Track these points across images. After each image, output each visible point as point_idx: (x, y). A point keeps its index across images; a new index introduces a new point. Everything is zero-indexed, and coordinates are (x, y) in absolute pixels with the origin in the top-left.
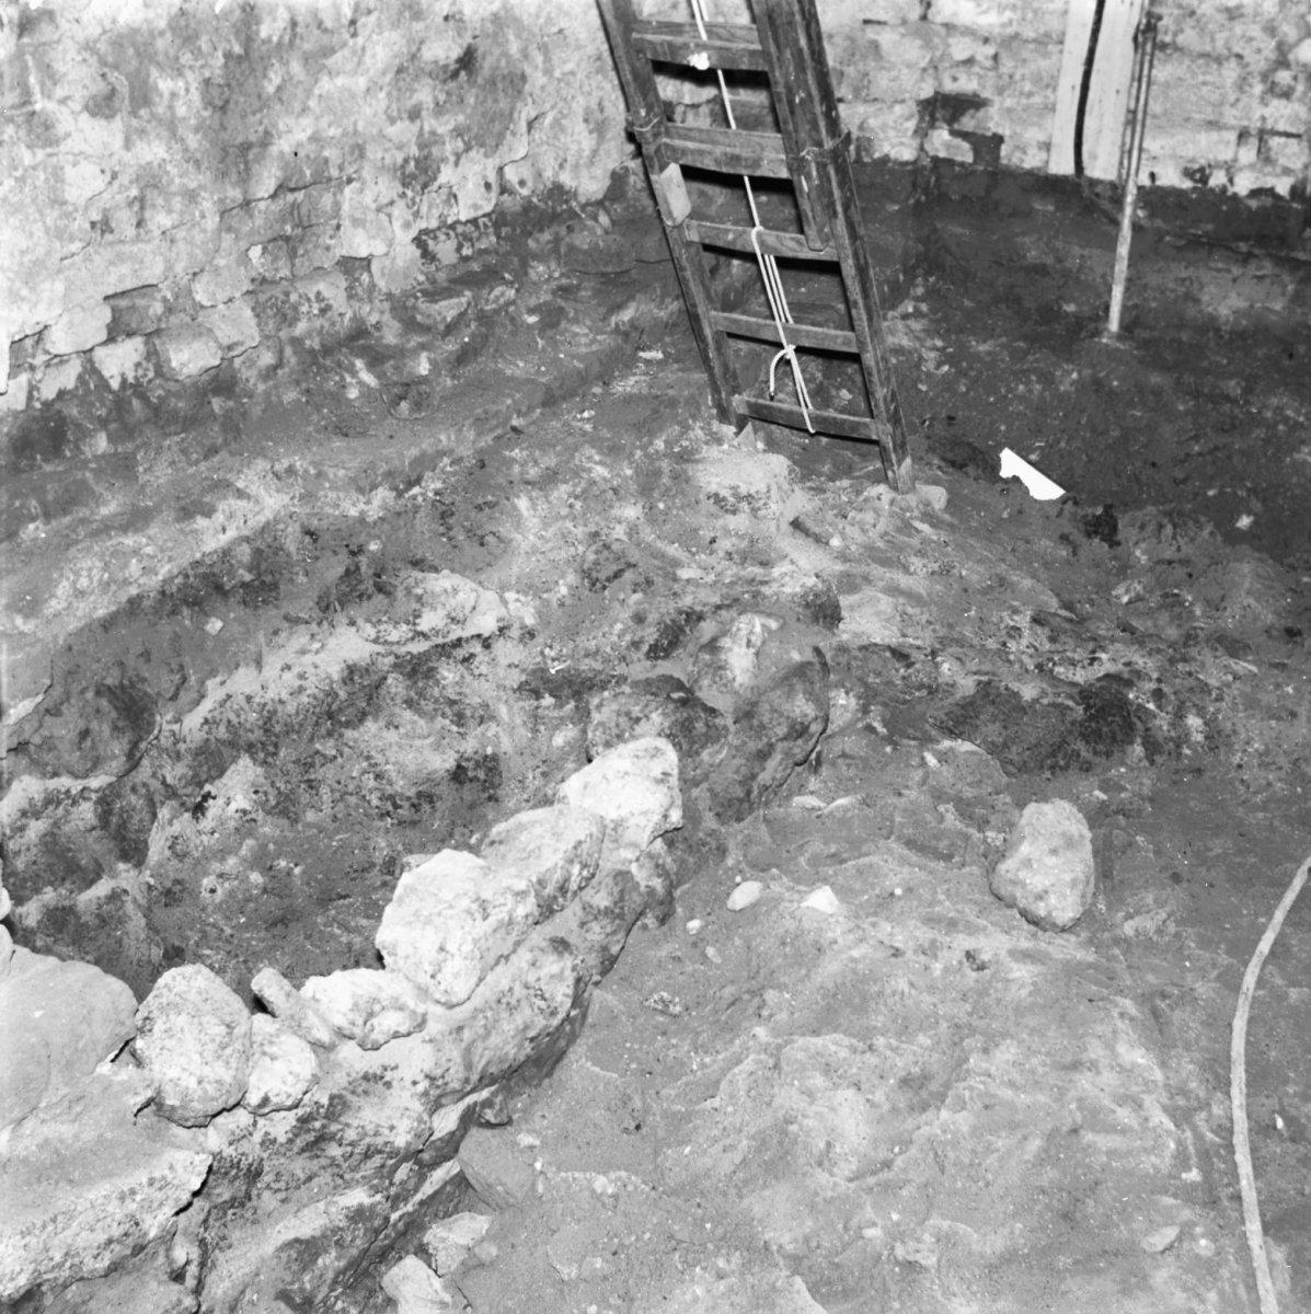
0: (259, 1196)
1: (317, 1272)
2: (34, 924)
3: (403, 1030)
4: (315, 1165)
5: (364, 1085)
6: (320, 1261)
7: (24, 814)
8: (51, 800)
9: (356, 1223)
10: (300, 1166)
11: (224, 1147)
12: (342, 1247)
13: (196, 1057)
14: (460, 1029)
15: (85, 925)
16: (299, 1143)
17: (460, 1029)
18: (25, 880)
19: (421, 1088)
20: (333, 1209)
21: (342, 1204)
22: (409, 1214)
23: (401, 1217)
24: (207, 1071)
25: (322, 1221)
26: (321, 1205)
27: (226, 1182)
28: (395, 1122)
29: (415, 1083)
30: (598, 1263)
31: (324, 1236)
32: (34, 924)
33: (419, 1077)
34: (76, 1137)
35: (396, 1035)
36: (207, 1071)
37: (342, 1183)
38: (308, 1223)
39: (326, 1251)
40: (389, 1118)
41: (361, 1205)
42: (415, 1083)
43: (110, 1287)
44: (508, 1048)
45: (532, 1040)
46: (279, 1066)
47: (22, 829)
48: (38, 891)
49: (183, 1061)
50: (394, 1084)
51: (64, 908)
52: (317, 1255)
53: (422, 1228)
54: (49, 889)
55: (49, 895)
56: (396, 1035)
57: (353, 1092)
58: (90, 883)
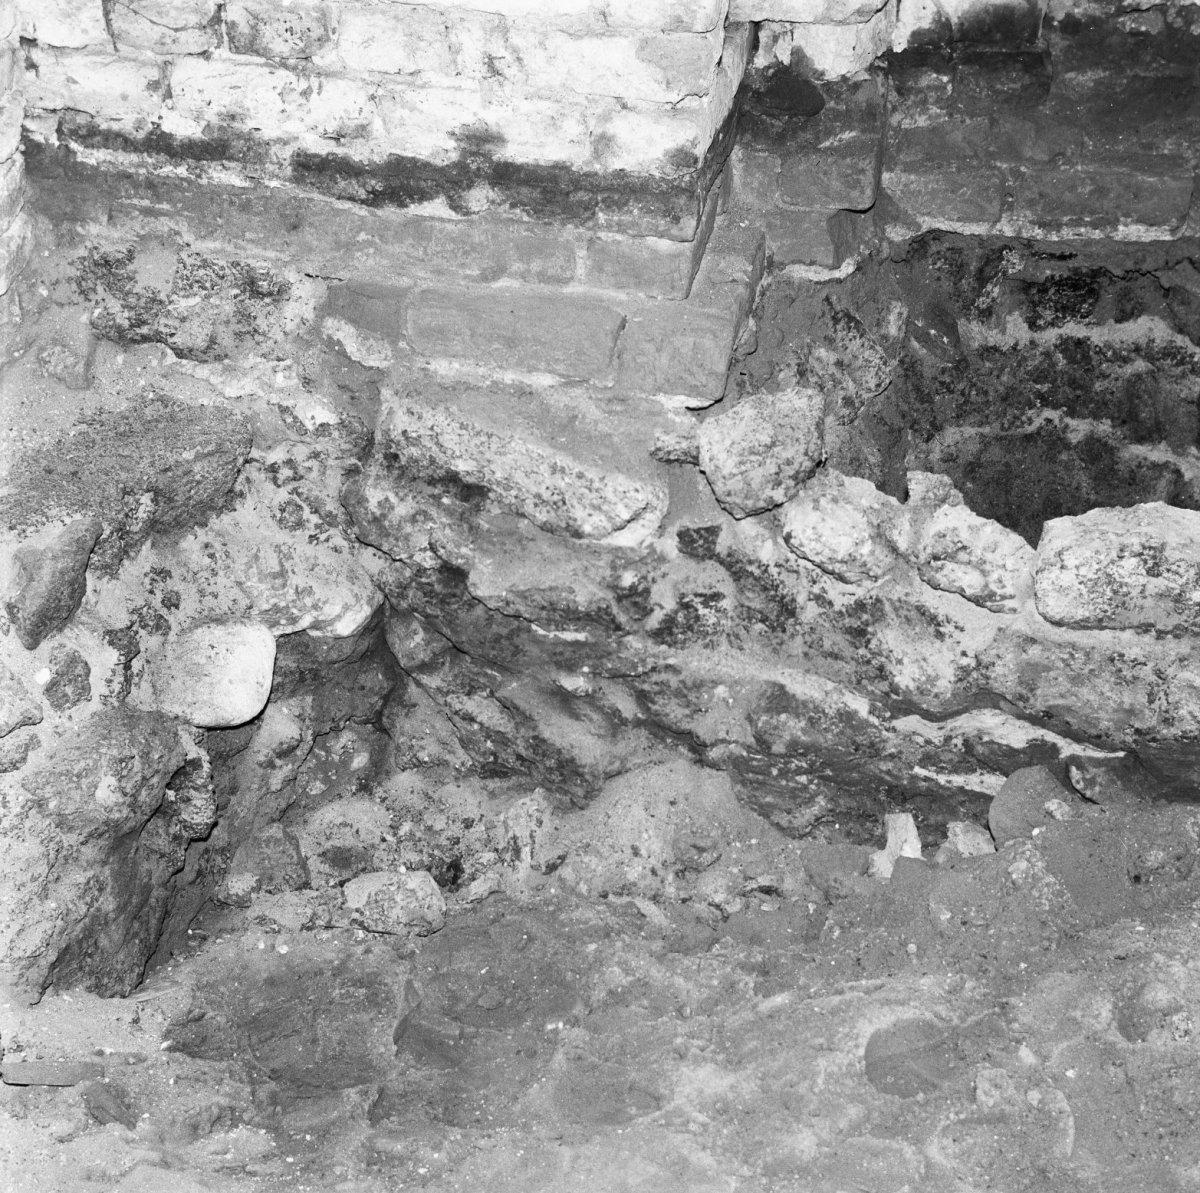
0: (792, 636)
1: (774, 721)
2: (1074, 441)
3: (969, 592)
4: (848, 652)
5: (913, 614)
6: (783, 717)
7: (1137, 349)
8: (1170, 352)
9: (841, 721)
10: (834, 640)
11: (772, 564)
12: (812, 724)
13: (728, 442)
14: (1033, 641)
15: (1113, 471)
16: (847, 621)
17: (1033, 641)
18: (1092, 400)
19: (964, 661)
20: (835, 697)
21: (845, 699)
22: (937, 783)
23: (926, 779)
24: (723, 456)
25: (818, 695)
26: (830, 686)
27: (763, 596)
28: (906, 661)
29: (964, 654)
30: (946, 916)
31: (804, 704)
32: (1074, 441)
33: (971, 653)
34: (596, 422)
35: (961, 592)
36: (723, 456)
37: (858, 685)
38: (803, 686)
39: (797, 716)
40: (905, 654)
41: (856, 712)
42: (964, 654)
43: (550, 546)
44: (1102, 714)
45: (1138, 731)
46: (814, 517)
47: (1126, 360)
48: (1096, 416)
49: (717, 437)
50: (948, 640)
51: (1106, 444)
52: (785, 710)
53: (954, 815)
54: (1109, 422)
55: (1104, 427)
56: (961, 592)
57: (896, 610)
58: (1140, 440)
